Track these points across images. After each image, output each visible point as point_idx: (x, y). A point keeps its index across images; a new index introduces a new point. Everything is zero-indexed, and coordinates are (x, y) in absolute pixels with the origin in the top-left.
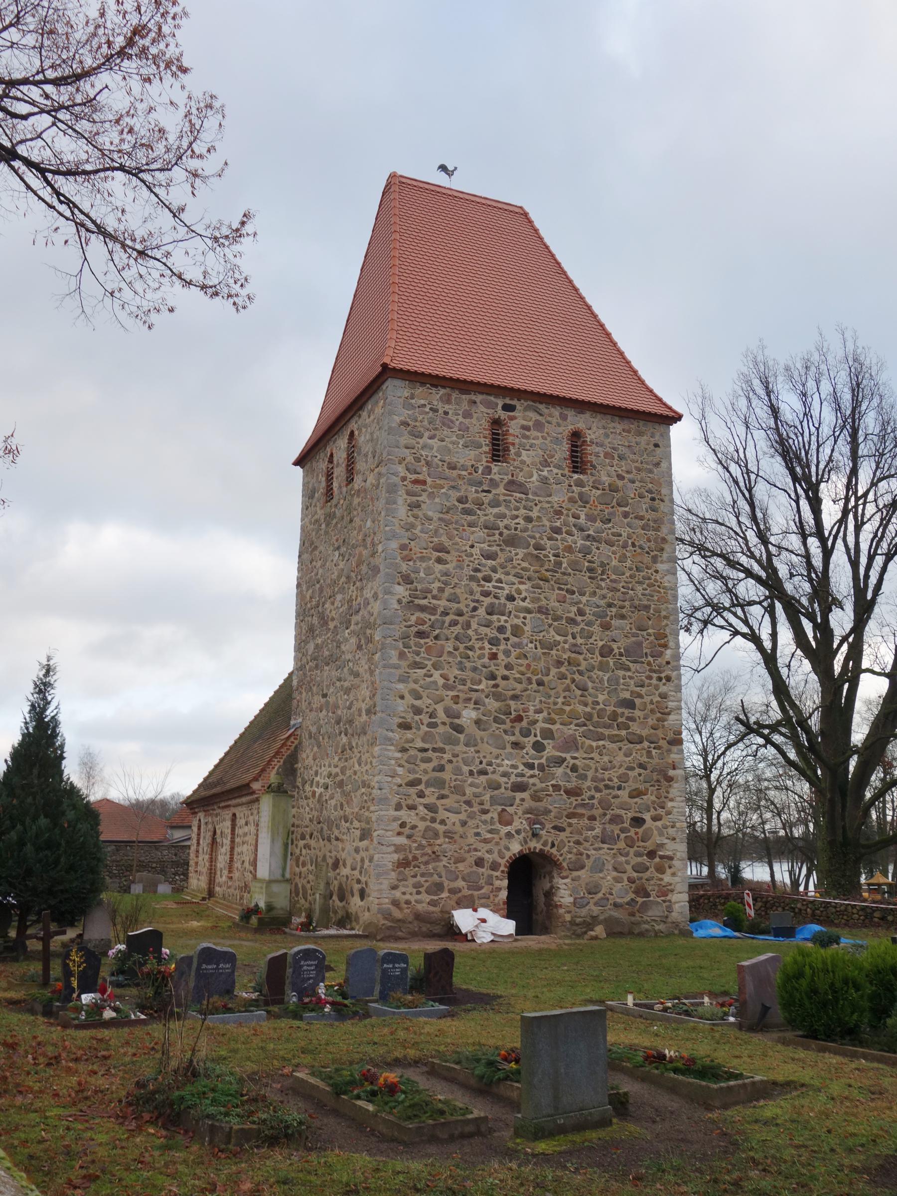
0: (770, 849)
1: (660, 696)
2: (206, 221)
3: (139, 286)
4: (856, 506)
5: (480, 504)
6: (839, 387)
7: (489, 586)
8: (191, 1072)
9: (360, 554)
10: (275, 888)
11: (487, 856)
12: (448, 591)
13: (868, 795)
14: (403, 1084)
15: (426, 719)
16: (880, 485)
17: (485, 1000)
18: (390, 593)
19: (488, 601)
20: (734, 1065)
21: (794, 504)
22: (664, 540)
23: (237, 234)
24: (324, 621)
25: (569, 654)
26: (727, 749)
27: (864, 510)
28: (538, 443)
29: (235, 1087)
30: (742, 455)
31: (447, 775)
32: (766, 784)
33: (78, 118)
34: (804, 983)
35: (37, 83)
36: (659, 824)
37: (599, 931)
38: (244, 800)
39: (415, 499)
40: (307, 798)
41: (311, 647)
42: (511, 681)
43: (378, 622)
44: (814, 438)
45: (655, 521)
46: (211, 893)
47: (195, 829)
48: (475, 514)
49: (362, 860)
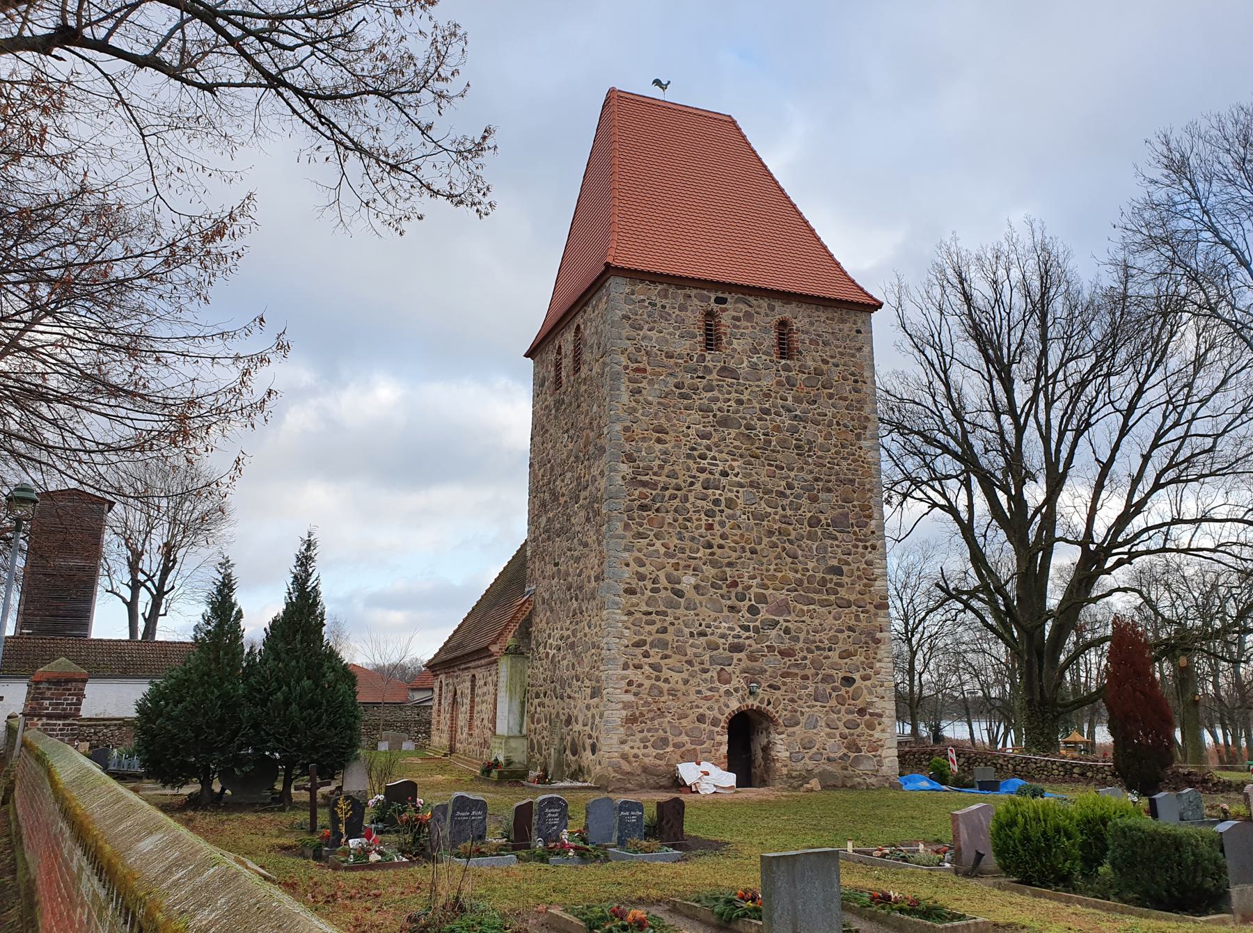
0: (968, 710)
1: (866, 563)
2: (452, 137)
3: (391, 197)
4: (1046, 386)
5: (695, 389)
6: (1028, 274)
7: (704, 463)
8: (458, 907)
9: (588, 436)
10: (513, 743)
11: (708, 712)
12: (667, 468)
13: (1062, 658)
14: (650, 919)
15: (650, 585)
16: (1069, 365)
17: (715, 847)
18: (615, 470)
19: (703, 476)
20: (954, 907)
21: (987, 384)
22: (866, 418)
23: (479, 148)
24: (555, 496)
25: (779, 524)
26: (927, 614)
27: (1053, 388)
28: (748, 332)
29: (499, 921)
30: (937, 340)
31: (668, 637)
32: (964, 647)
33: (335, 47)
34: (1017, 831)
35: (299, 18)
36: (868, 683)
37: (814, 783)
38: (483, 662)
39: (636, 385)
40: (540, 659)
41: (543, 520)
42: (727, 549)
43: (605, 497)
44: (1005, 323)
45: (858, 402)
46: (452, 750)
47: (437, 690)
48: (691, 398)
49: (593, 716)
